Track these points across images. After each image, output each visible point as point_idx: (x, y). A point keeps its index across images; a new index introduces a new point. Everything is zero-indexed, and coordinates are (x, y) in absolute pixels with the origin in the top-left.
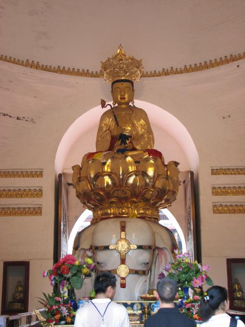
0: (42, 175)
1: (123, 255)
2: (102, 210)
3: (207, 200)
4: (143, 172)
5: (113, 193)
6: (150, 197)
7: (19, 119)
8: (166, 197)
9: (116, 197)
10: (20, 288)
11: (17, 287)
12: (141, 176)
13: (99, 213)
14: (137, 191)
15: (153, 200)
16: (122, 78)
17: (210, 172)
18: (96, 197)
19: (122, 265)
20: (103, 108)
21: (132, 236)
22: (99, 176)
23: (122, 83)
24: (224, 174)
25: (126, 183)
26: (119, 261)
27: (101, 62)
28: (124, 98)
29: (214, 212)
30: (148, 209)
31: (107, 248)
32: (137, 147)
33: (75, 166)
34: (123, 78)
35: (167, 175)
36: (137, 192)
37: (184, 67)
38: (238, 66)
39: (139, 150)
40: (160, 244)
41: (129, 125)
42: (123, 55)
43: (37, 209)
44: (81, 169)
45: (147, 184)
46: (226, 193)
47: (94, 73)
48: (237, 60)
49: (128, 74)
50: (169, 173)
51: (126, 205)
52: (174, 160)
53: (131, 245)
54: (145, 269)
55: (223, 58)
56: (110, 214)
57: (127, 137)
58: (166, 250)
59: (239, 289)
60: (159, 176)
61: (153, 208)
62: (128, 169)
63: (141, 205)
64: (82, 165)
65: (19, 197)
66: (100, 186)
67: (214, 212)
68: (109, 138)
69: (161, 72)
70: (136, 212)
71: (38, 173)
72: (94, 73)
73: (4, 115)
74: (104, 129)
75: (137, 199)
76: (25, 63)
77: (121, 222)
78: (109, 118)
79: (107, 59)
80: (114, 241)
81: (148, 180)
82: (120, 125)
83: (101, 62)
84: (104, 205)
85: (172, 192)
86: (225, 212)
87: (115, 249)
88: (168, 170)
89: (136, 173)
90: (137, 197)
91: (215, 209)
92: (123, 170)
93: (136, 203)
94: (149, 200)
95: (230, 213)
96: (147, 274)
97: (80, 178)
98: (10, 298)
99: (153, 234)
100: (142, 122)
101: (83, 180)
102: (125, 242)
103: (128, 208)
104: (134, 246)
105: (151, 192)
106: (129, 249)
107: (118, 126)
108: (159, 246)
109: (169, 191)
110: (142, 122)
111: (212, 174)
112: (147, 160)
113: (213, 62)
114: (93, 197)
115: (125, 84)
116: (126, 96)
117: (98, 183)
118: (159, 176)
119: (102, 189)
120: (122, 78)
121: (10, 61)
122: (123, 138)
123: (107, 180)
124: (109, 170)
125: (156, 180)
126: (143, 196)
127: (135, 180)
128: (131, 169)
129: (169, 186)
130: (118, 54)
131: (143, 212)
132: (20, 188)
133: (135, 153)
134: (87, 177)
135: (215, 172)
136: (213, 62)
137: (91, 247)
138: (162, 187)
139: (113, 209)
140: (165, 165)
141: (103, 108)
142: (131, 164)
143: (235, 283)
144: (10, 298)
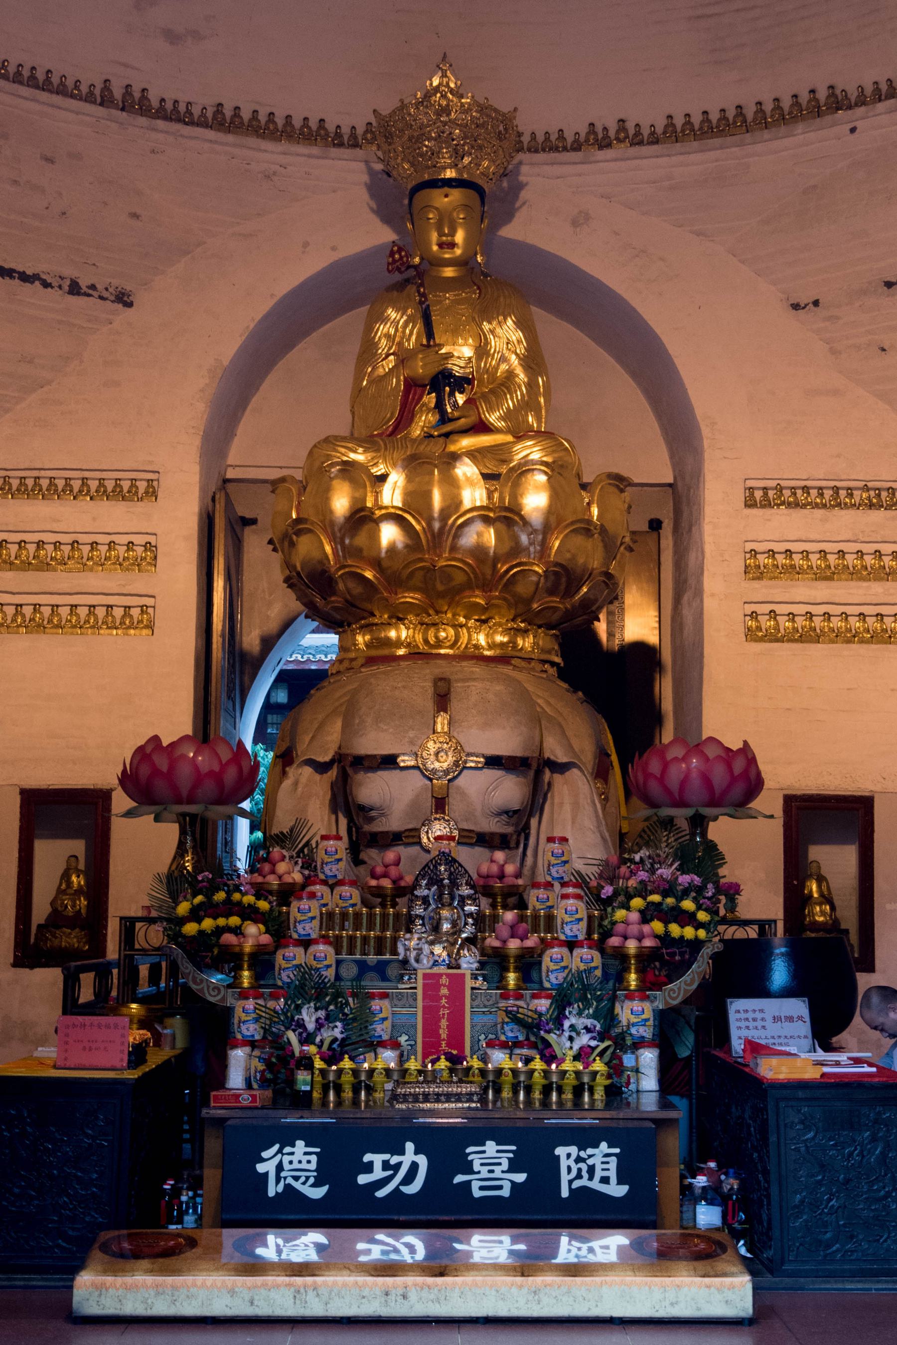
0: (155, 494)
2: (371, 632)
7: (78, 293)
10: (74, 878)
11: (66, 876)
13: (360, 639)
22: (362, 518)
23: (446, 190)
24: (789, 505)
31: (389, 762)
34: (450, 174)
37: (665, 122)
38: (853, 130)
41: (466, 340)
42: (451, 91)
47: (346, 131)
48: (850, 107)
49: (466, 160)
51: (449, 615)
52: (615, 470)
54: (509, 830)
56: (398, 643)
57: (461, 383)
59: (822, 895)
67: (752, 635)
68: (396, 383)
69: (582, 138)
72: (346, 131)
76: (97, 92)
81: (524, 539)
84: (377, 613)
89: (485, 516)
90: (486, 586)
91: (752, 624)
96: (513, 844)
98: (40, 911)
103: (457, 626)
115: (456, 195)
117: (361, 540)
121: (46, 86)
122: (444, 381)
123: (389, 534)
130: (437, 89)
131: (505, 639)
133: (485, 440)
139: (408, 628)
143: (810, 876)
144: (40, 911)
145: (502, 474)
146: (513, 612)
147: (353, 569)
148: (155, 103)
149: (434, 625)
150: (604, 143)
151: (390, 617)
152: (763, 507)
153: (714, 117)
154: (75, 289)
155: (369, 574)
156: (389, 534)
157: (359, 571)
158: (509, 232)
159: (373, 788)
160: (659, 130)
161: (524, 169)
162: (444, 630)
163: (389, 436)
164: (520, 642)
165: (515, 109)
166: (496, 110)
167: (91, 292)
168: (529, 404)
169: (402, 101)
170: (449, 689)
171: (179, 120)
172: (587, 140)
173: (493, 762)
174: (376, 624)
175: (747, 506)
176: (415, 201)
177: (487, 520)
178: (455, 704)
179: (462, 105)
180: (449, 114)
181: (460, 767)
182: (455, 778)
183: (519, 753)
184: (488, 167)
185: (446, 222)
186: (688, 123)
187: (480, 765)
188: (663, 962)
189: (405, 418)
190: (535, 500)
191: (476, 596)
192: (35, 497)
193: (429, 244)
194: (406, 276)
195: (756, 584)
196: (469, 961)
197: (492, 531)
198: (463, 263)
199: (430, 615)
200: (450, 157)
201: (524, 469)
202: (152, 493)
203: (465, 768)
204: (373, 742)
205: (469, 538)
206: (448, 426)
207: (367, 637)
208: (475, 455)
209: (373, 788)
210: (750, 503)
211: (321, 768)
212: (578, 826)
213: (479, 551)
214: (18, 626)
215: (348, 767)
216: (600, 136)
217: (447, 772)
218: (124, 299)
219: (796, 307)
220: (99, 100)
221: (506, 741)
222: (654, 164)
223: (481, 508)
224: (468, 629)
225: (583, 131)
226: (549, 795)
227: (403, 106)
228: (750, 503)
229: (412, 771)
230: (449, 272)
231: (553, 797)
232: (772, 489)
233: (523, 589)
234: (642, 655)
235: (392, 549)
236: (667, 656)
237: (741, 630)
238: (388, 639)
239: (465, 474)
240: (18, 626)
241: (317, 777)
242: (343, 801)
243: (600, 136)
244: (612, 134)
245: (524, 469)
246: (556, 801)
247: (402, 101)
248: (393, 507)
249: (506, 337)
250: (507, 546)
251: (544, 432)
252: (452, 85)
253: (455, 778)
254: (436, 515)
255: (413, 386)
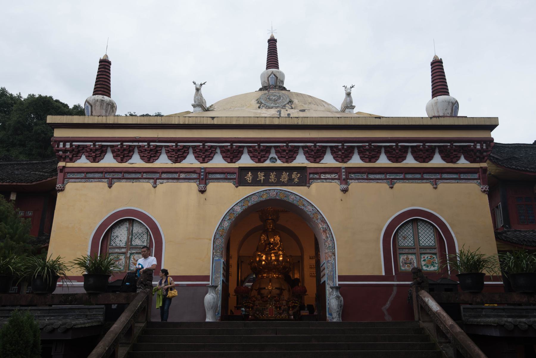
22: (261, 261)
57: (272, 244)
122: (270, 244)
145: (277, 256)
158: (278, 223)
159: (263, 291)
163: (263, 252)
168: (280, 247)
173: (276, 288)
181: (272, 289)
188: (293, 307)
189: (265, 248)
194: (265, 231)
196: (274, 307)
198: (272, 229)
201: (280, 255)
204: (262, 286)
205: (273, 263)
206: (271, 249)
208: (274, 253)
209: (263, 291)
210: (310, 258)
212: (286, 295)
213: (274, 265)
215: (260, 289)
221: (278, 286)
234: (297, 280)
236: (301, 280)
242: (259, 293)
245: (280, 255)
249: (277, 238)
255: (266, 245)
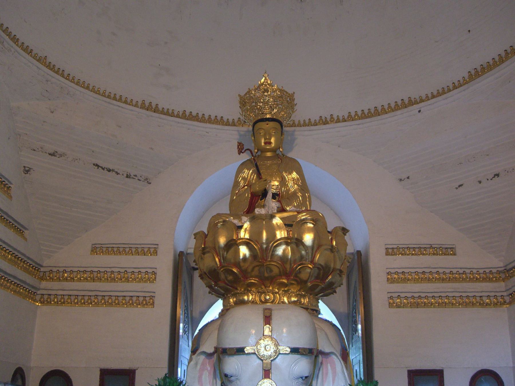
1: (267, 363)
2: (236, 297)
3: (379, 289)
4: (297, 239)
5: (253, 270)
6: (307, 277)
8: (330, 277)
9: (256, 277)
12: (294, 246)
13: (231, 300)
14: (288, 266)
15: (311, 282)
16: (266, 131)
17: (384, 251)
18: (226, 278)
19: (266, 380)
20: (239, 154)
21: (282, 332)
22: (233, 244)
23: (267, 122)
24: (402, 254)
25: (273, 255)
26: (261, 373)
27: (239, 95)
28: (270, 143)
29: (391, 305)
30: (304, 296)
31: (240, 351)
32: (288, 209)
33: (199, 233)
34: (268, 116)
35: (332, 246)
36: (288, 270)
38: (419, 111)
39: (290, 211)
40: (324, 346)
43: (147, 299)
44: (206, 236)
45: (302, 257)
46: (405, 280)
47: (231, 121)
49: (275, 110)
50: (334, 243)
51: (271, 288)
53: (279, 347)
55: (399, 103)
58: (334, 356)
60: (319, 246)
61: (311, 294)
62: (275, 235)
63: (294, 289)
64: (208, 232)
65: (123, 282)
66: (232, 261)
67: (391, 305)
68: (248, 195)
69: (317, 122)
70: (286, 299)
71: (152, 250)
72: (231, 121)
73: (109, 170)
74: (242, 184)
75: (288, 280)
77: (265, 309)
78: (249, 169)
79: (247, 90)
80: (252, 340)
82: (264, 177)
83: (239, 95)
84: (239, 288)
85: (338, 272)
86: (405, 306)
87: (255, 353)
88: (332, 236)
89: (287, 241)
90: (287, 275)
91: (391, 301)
92: (267, 235)
93: (285, 285)
94: (306, 282)
95: (411, 307)
97: (204, 249)
99: (315, 331)
100: (294, 175)
101: (209, 252)
102: (270, 342)
103: (274, 293)
104: (285, 349)
105: (309, 270)
106: (278, 353)
107: (261, 178)
108: (323, 350)
109: (334, 270)
110: (294, 175)
111: (386, 255)
112: (304, 222)
113: (386, 107)
114: (222, 276)
115: (271, 124)
116: (273, 140)
117: (230, 255)
118: (319, 246)
119: (237, 264)
120: (266, 131)
123: (244, 251)
124: (247, 236)
125: (316, 251)
126: (296, 276)
127: (284, 251)
128: (280, 234)
129: (335, 262)
130: (262, 84)
132: (127, 269)
133: (285, 215)
134: (215, 249)
135: (391, 252)
136: (386, 107)
137: (216, 349)
138: (326, 264)
139: (252, 295)
140: (329, 232)
141: (239, 154)
142: (279, 228)
146: (299, 286)
147: (228, 268)
148: (161, 109)
149: (264, 293)
150: (326, 123)
151: (245, 290)
152: (392, 255)
153: (366, 112)
154: (128, 176)
155: (235, 270)
156: (244, 251)
157: (230, 268)
160: (346, 117)
161: (296, 133)
162: (269, 295)
164: (303, 300)
165: (294, 93)
166: (286, 92)
167: (135, 177)
169: (249, 89)
170: (271, 313)
171: (169, 115)
172: (319, 122)
174: (238, 293)
175: (386, 255)
176: (255, 128)
177: (287, 244)
178: (274, 321)
179: (273, 89)
180: (268, 92)
182: (274, 359)
183: (307, 346)
184: (283, 115)
185: (268, 135)
186: (356, 114)
187: (287, 352)
190: (308, 238)
191: (283, 279)
192: (111, 254)
193: (261, 143)
195: (392, 285)
197: (289, 248)
199: (262, 288)
200: (269, 109)
202: (156, 253)
203: (280, 354)
207: (235, 299)
210: (387, 254)
211: (209, 355)
214: (103, 304)
216: (324, 120)
217: (270, 356)
218: (148, 181)
219: (401, 180)
220: (140, 107)
222: (343, 128)
223: (285, 238)
224: (279, 295)
225: (318, 119)
226: (321, 369)
227: (249, 92)
228: (387, 254)
229: (252, 355)
230: (269, 154)
231: (323, 370)
232: (395, 248)
233: (304, 276)
235: (245, 258)
237: (388, 303)
238: (244, 300)
239: (277, 224)
240: (103, 304)
241: (207, 361)
243: (324, 120)
244: (328, 120)
246: (324, 372)
247: (249, 89)
248: (245, 239)
250: (297, 256)
251: (310, 210)
252: (269, 82)
253: (274, 359)
254: (264, 241)
